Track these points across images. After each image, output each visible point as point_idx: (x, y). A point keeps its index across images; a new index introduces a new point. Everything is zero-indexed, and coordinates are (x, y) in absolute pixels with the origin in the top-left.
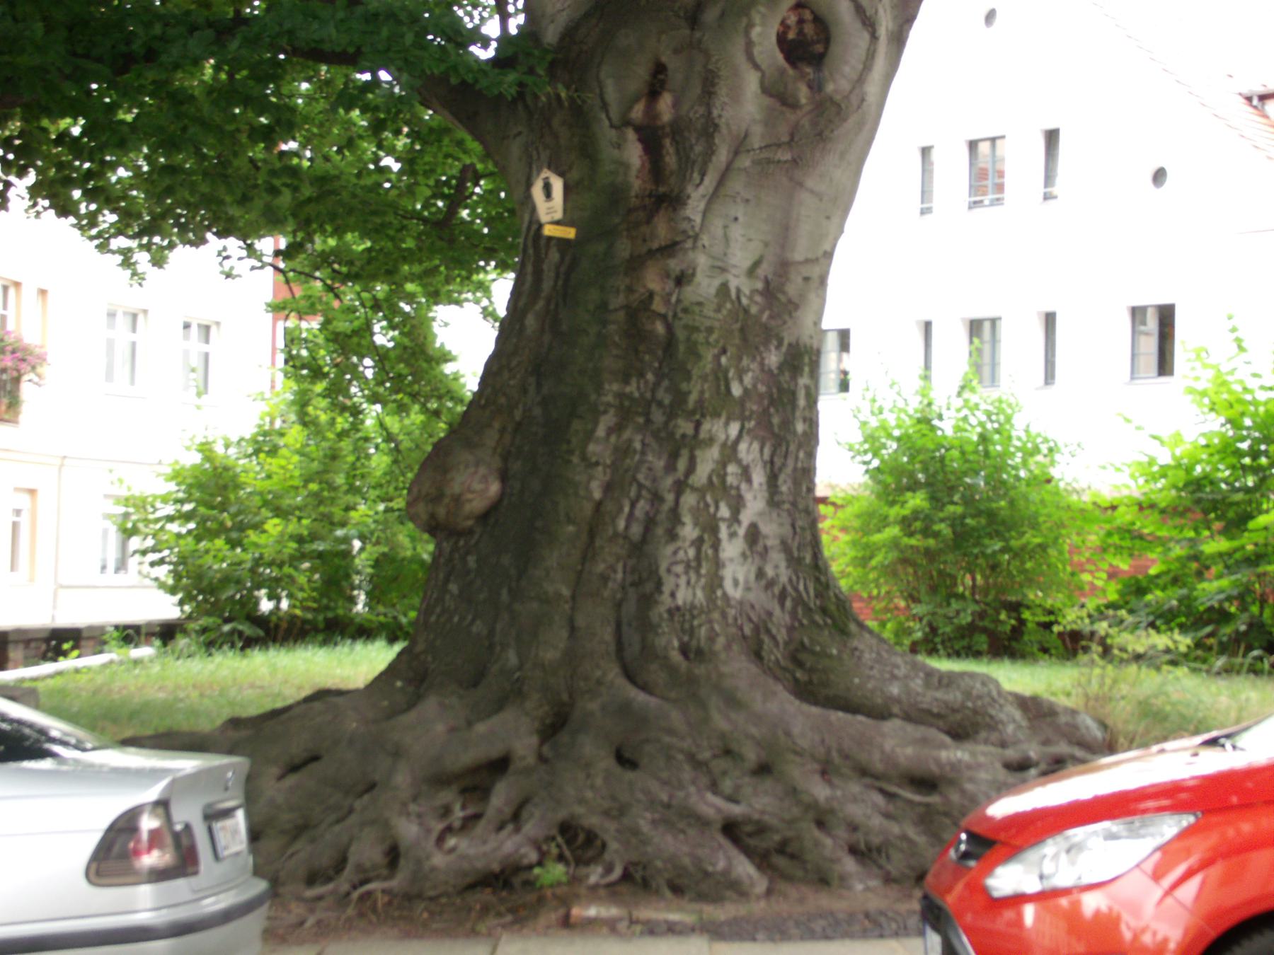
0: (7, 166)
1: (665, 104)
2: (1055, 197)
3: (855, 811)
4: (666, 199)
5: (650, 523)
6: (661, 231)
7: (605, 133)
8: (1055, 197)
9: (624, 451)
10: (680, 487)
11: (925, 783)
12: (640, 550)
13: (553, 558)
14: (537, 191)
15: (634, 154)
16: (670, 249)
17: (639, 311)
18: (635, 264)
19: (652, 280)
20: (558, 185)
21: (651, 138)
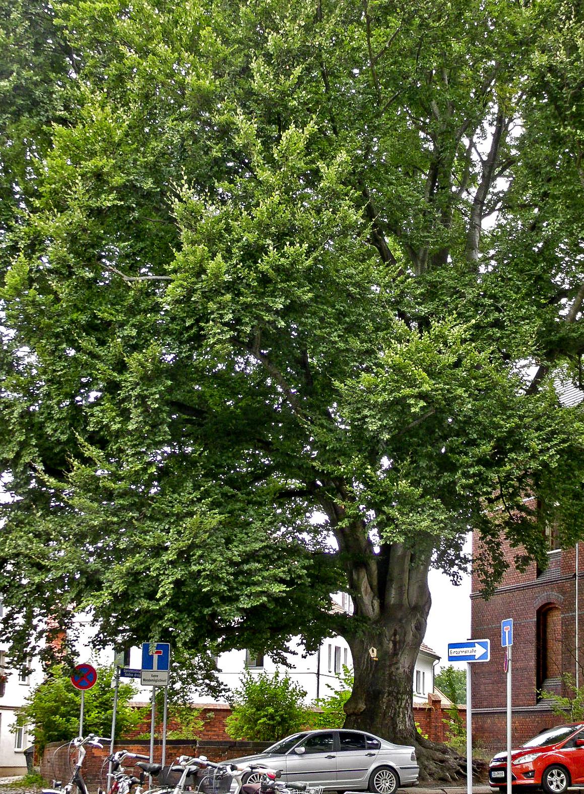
0: (256, 5)
1: (397, 637)
2: (35, 670)
3: (431, 767)
4: (395, 654)
5: (395, 714)
6: (395, 660)
7: (386, 641)
8: (35, 670)
9: (389, 701)
10: (399, 707)
11: (442, 761)
12: (393, 719)
13: (378, 720)
14: (370, 651)
15: (391, 645)
16: (396, 663)
17: (391, 674)
18: (390, 666)
19: (393, 669)
20: (375, 650)
21: (395, 643)
